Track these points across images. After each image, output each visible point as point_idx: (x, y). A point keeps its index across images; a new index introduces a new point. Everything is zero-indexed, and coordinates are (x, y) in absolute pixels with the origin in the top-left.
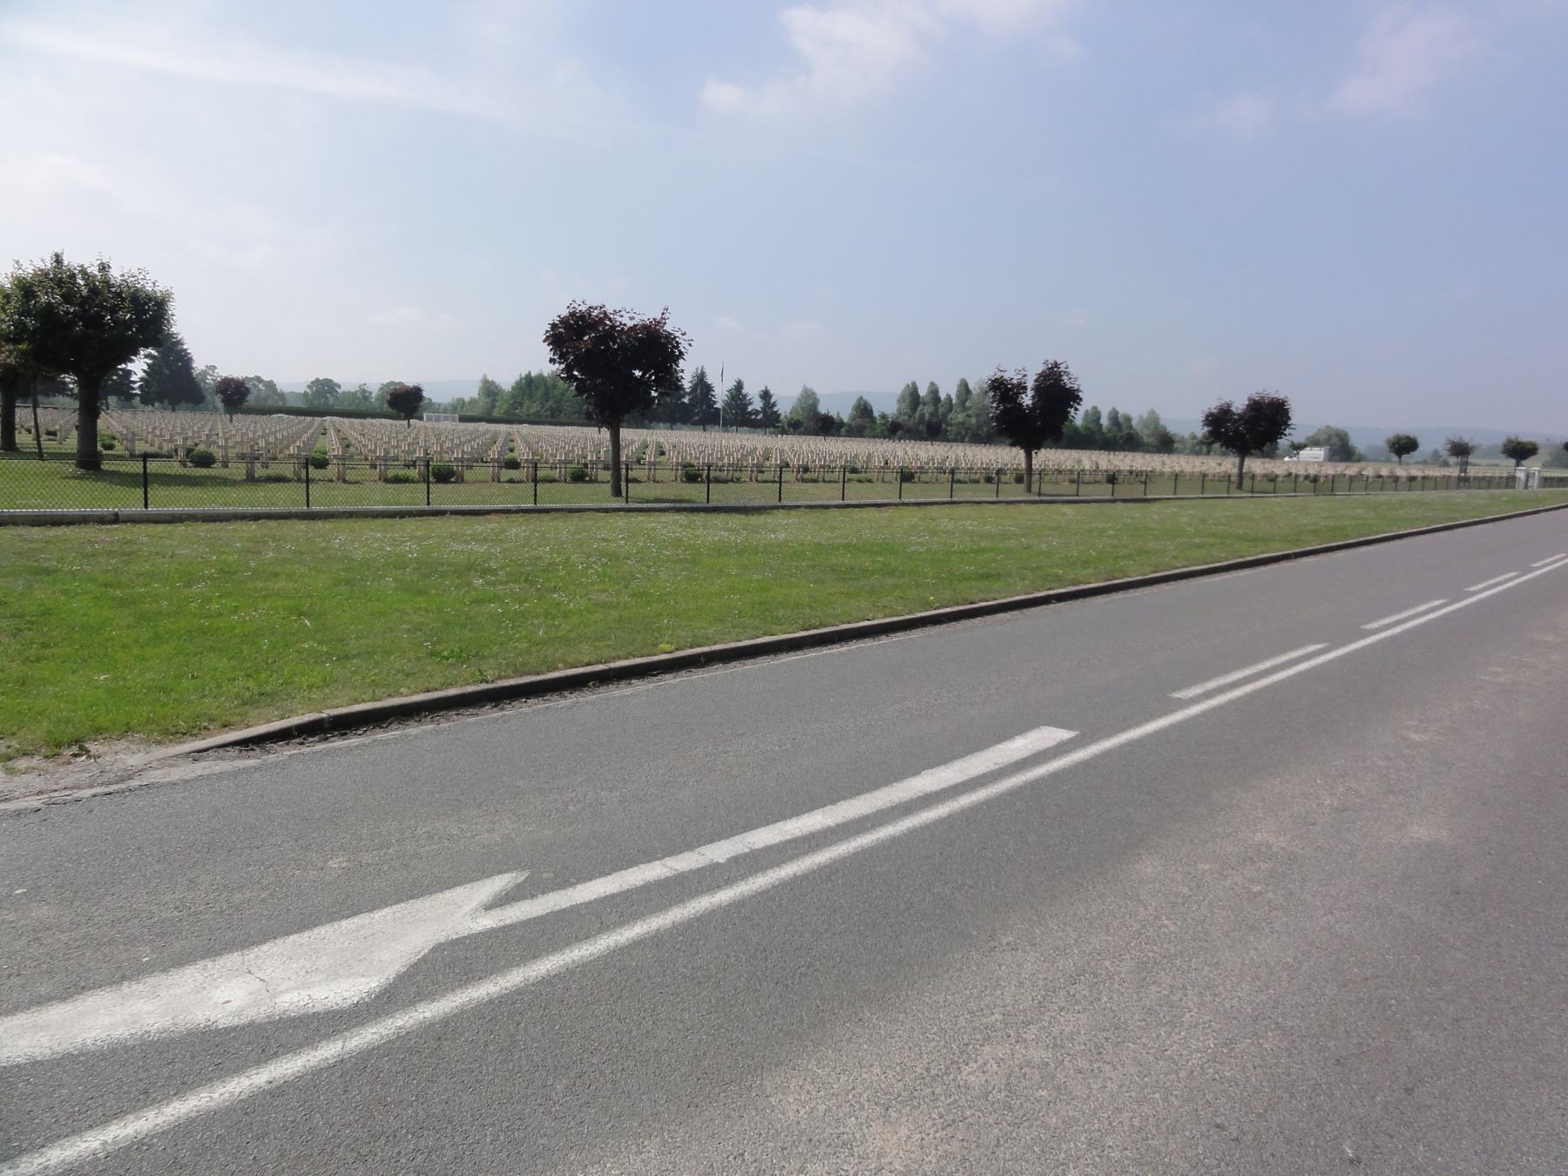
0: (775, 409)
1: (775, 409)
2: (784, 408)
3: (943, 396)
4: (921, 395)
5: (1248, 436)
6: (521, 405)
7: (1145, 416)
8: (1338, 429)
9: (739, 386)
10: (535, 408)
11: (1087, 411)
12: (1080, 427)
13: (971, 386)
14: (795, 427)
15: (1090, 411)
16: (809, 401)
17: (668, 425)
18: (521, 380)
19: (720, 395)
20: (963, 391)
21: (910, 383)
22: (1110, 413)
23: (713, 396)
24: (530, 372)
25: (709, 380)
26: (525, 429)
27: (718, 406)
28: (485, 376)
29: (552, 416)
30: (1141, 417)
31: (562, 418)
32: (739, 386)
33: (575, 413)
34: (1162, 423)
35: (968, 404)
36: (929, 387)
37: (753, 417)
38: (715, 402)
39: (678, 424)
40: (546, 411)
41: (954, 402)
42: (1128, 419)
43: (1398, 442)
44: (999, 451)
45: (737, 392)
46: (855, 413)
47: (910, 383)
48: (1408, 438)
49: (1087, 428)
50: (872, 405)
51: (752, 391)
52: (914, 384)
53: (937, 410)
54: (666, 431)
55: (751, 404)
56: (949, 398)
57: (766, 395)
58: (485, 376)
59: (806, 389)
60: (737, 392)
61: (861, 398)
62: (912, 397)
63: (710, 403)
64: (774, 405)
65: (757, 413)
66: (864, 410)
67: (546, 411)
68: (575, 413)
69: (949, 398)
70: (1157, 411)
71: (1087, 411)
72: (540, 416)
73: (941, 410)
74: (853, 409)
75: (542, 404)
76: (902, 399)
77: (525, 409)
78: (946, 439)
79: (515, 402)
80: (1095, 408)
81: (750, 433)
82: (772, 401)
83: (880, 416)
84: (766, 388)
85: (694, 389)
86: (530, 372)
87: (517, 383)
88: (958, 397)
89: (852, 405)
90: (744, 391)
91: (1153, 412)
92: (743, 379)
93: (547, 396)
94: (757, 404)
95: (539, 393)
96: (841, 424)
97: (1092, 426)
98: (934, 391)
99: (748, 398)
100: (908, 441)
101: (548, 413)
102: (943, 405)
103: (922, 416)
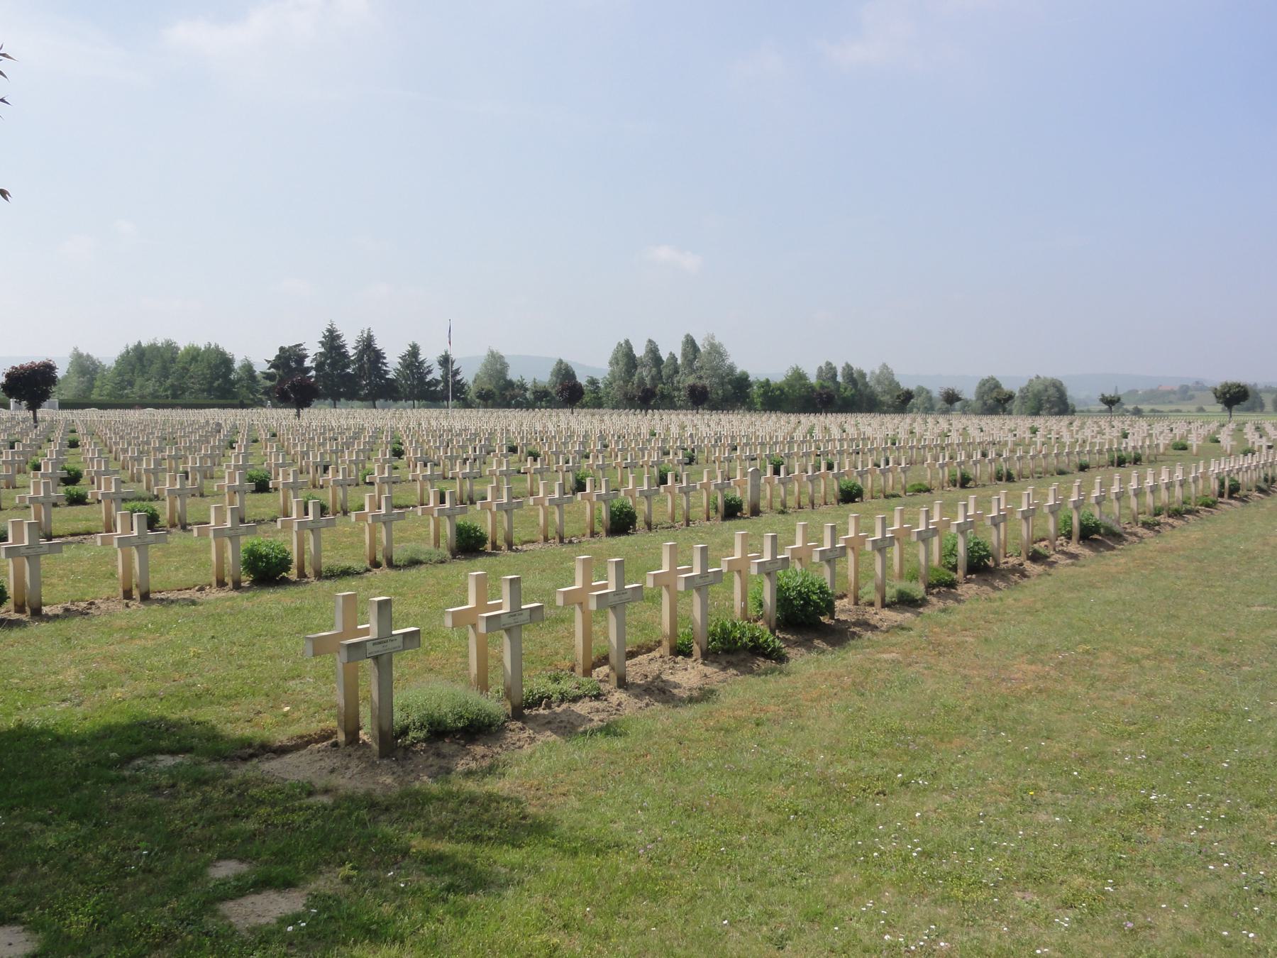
0: (459, 378)
1: (459, 378)
2: (468, 375)
3: (665, 356)
4: (638, 355)
5: (313, 373)
6: (131, 384)
7: (877, 372)
8: (1053, 379)
9: (414, 352)
10: (151, 386)
11: (821, 367)
12: (814, 384)
13: (699, 343)
14: (540, 399)
15: (824, 368)
16: (496, 365)
17: (329, 401)
18: (128, 352)
19: (393, 361)
20: (690, 350)
21: (622, 342)
22: (844, 369)
23: (385, 364)
24: (140, 343)
25: (379, 344)
26: (92, 414)
27: (390, 376)
28: (76, 349)
29: (175, 396)
30: (872, 373)
31: (188, 397)
32: (414, 352)
33: (203, 391)
34: (897, 379)
35: (697, 364)
36: (647, 346)
37: (433, 388)
38: (386, 372)
39: (342, 400)
40: (166, 390)
41: (679, 362)
42: (863, 375)
43: (1228, 392)
44: (764, 418)
45: (412, 358)
46: (554, 379)
47: (622, 342)
48: (1239, 386)
49: (822, 387)
50: (574, 369)
51: (430, 356)
52: (627, 342)
53: (659, 372)
54: (368, 411)
55: (430, 372)
56: (673, 357)
57: (445, 361)
58: (76, 349)
59: (492, 352)
60: (412, 358)
61: (561, 362)
62: (626, 359)
63: (381, 374)
64: (456, 373)
65: (437, 382)
66: (565, 375)
67: (166, 390)
68: (203, 391)
69: (673, 357)
70: (565, 360)
71: (821, 367)
72: (157, 397)
73: (665, 372)
74: (552, 375)
75: (159, 381)
76: (615, 361)
77: (136, 389)
78: (751, 408)
79: (123, 381)
80: (828, 364)
81: (428, 407)
82: (455, 368)
83: (588, 381)
84: (446, 352)
85: (361, 354)
86: (140, 343)
87: (122, 356)
88: (684, 355)
89: (551, 370)
90: (421, 358)
91: (885, 366)
92: (419, 344)
93: (165, 373)
94: (437, 373)
95: (157, 366)
96: (882, 403)
97: (829, 384)
98: (653, 350)
99: (425, 365)
100: (638, 411)
101: (169, 393)
102: (666, 366)
103: (642, 380)
